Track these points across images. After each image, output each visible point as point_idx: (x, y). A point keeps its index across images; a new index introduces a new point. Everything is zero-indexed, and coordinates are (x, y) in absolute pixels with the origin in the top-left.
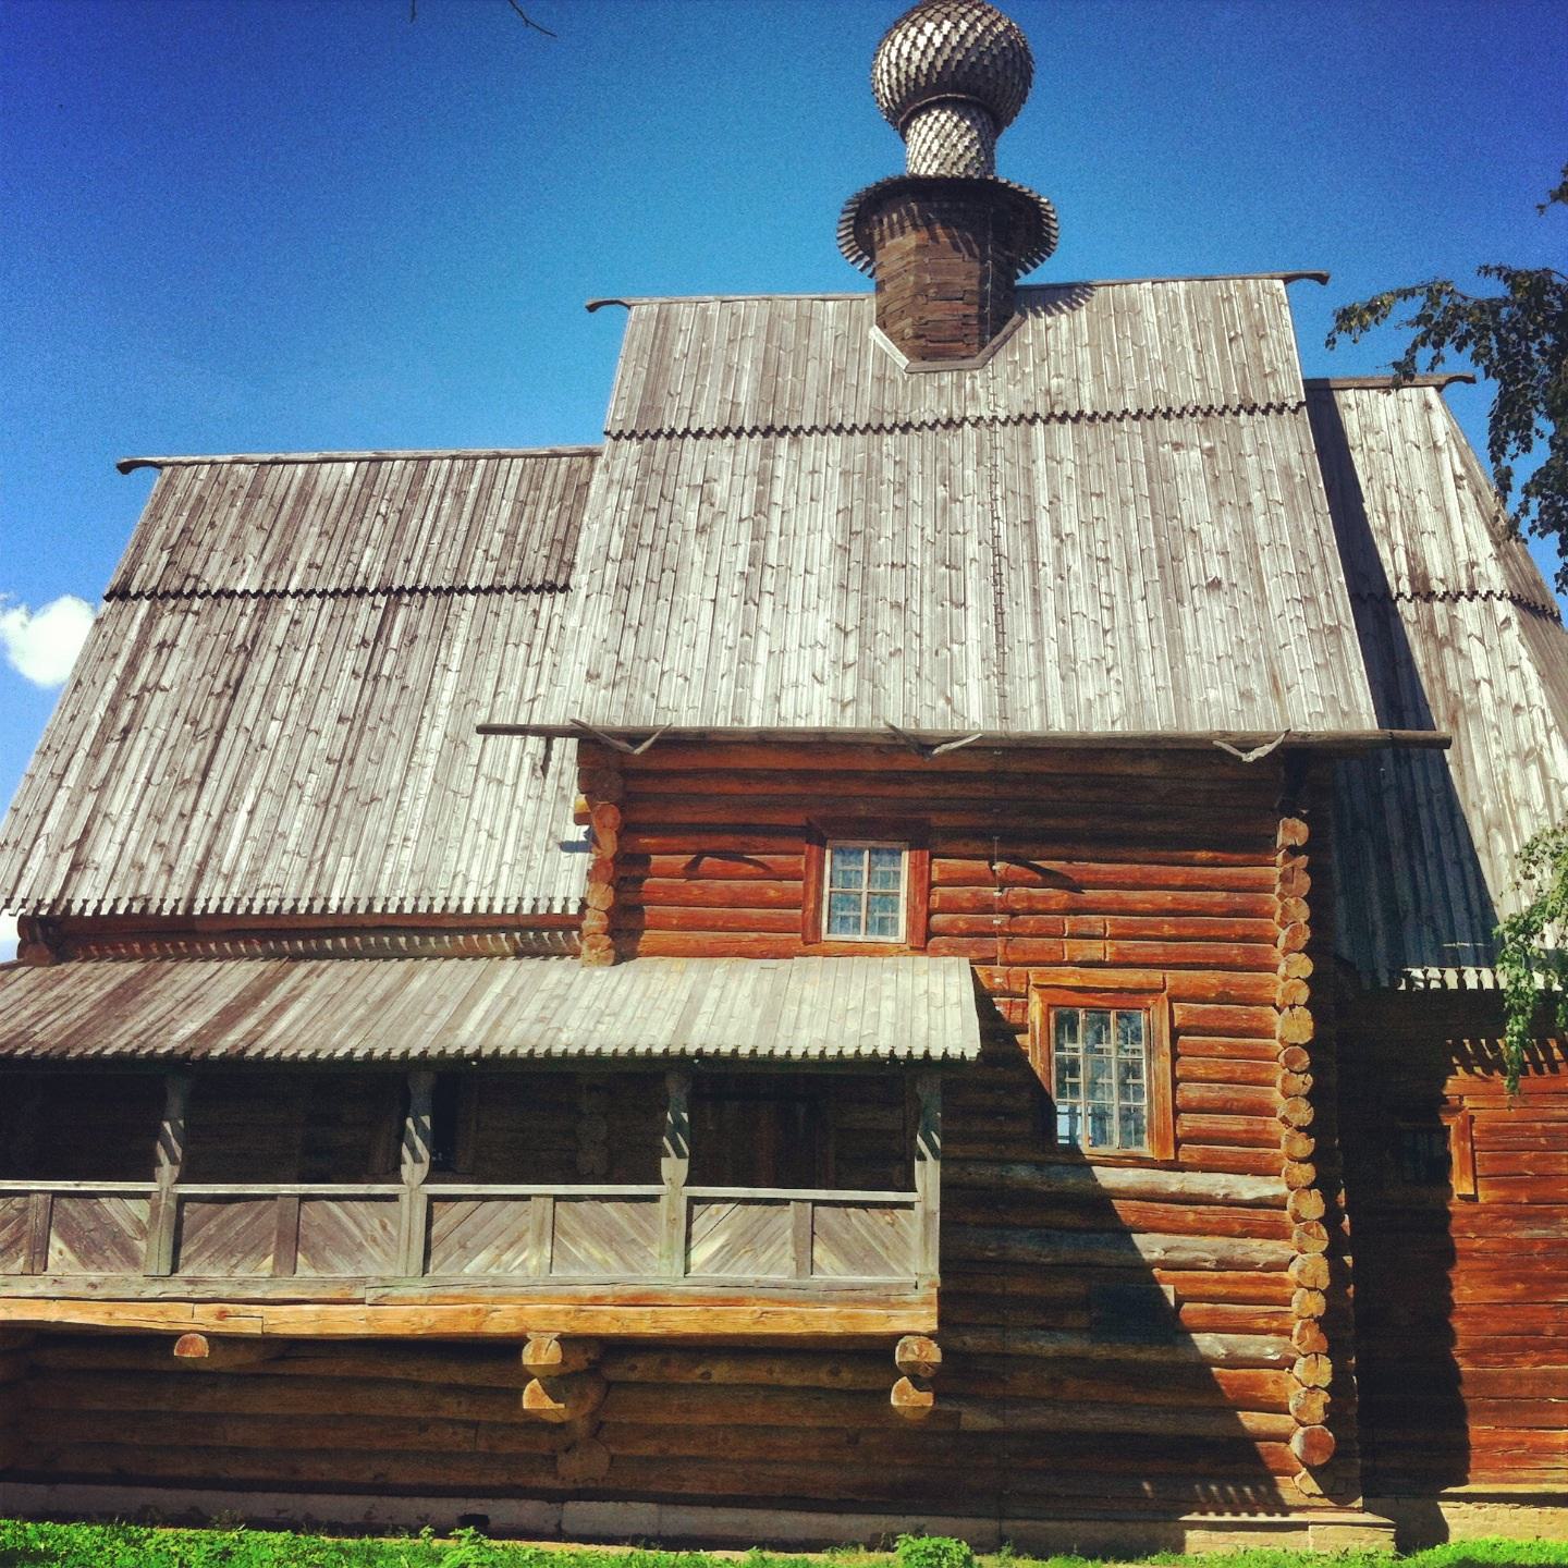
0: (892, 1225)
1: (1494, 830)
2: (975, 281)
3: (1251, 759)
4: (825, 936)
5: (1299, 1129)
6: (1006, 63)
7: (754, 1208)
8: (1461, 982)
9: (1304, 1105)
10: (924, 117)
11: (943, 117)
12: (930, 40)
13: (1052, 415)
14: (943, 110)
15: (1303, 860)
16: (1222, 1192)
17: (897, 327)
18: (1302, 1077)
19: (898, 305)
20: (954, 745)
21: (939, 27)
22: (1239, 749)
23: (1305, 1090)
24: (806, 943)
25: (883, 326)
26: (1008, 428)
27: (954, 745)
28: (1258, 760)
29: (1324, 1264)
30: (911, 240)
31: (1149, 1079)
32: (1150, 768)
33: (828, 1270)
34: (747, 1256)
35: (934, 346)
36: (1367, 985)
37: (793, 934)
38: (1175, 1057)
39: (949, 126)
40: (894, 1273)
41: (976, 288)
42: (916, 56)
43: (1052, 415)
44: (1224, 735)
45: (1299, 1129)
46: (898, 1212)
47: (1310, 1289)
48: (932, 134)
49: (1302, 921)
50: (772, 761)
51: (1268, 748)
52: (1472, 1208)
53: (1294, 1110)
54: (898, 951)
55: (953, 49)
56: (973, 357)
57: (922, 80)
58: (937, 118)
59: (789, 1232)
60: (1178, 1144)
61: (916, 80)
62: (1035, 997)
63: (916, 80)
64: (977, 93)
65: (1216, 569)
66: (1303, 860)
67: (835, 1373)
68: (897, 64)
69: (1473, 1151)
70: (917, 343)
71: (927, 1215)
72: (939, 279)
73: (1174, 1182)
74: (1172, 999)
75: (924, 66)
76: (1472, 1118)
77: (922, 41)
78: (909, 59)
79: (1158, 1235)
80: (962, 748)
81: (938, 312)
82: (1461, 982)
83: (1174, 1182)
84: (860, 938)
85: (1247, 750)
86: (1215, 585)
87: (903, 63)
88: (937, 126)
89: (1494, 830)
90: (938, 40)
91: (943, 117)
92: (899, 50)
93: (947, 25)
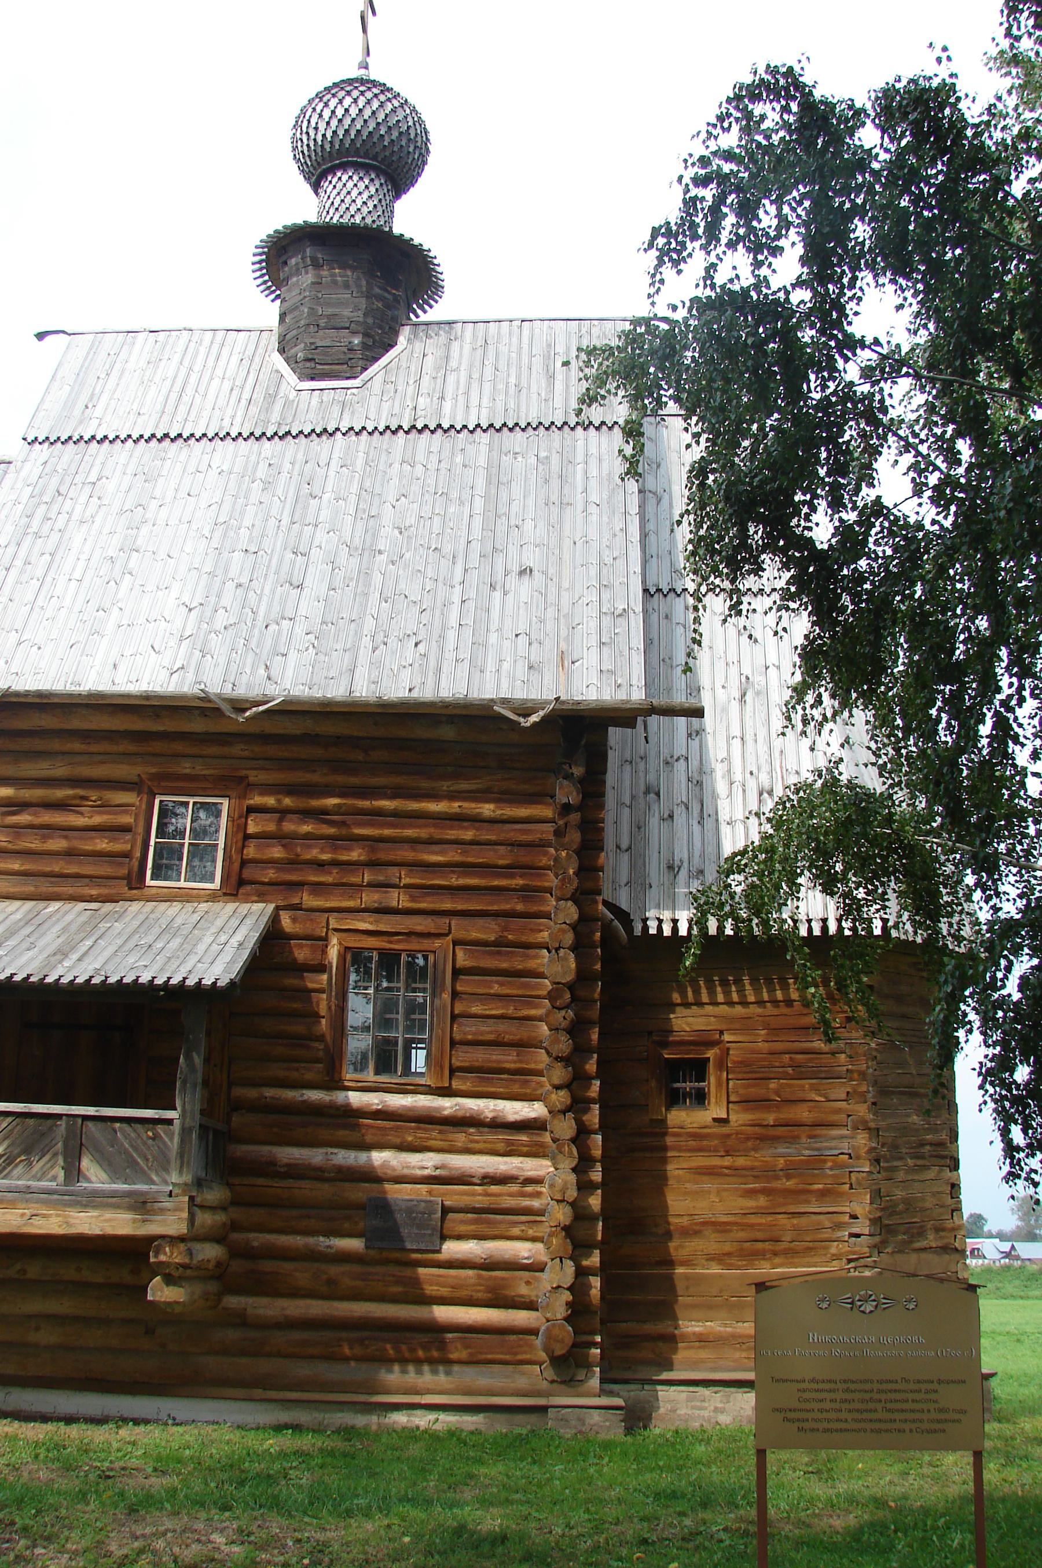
0: (153, 1139)
1: (765, 795)
2: (360, 313)
3: (528, 724)
4: (149, 882)
5: (557, 1059)
6: (401, 133)
7: (31, 1122)
8: (721, 928)
9: (563, 1037)
10: (339, 174)
11: (345, 178)
12: (333, 112)
13: (414, 427)
14: (367, 173)
15: (575, 817)
16: (490, 1115)
17: (293, 351)
18: (563, 1012)
19: (294, 333)
20: (261, 708)
21: (341, 102)
22: (519, 715)
23: (564, 1024)
24: (131, 888)
25: (282, 351)
26: (411, 436)
27: (261, 708)
28: (535, 724)
29: (572, 1178)
30: (308, 278)
31: (432, 1016)
32: (447, 733)
33: (94, 1179)
34: (21, 1166)
35: (316, 365)
36: (638, 930)
37: (121, 878)
38: (455, 995)
39: (350, 184)
40: (153, 1183)
41: (361, 319)
42: (322, 126)
43: (414, 427)
44: (505, 701)
45: (557, 1059)
46: (160, 1129)
47: (558, 1201)
48: (335, 192)
49: (571, 871)
50: (308, 726)
51: (541, 713)
52: (725, 1130)
53: (557, 1041)
54: (212, 897)
55: (340, 121)
56: (355, 378)
57: (327, 147)
58: (350, 177)
59: (60, 1145)
60: (452, 1071)
61: (322, 146)
62: (334, 941)
63: (322, 146)
64: (375, 158)
65: (531, 558)
66: (575, 817)
67: (79, 1270)
68: (307, 133)
69: (728, 1079)
70: (308, 364)
71: (185, 1131)
72: (330, 311)
73: (447, 1105)
74: (455, 943)
75: (329, 135)
76: (728, 1049)
77: (327, 114)
78: (316, 129)
79: (431, 1155)
80: (264, 712)
81: (324, 339)
82: (721, 928)
83: (447, 1105)
84: (182, 884)
85: (526, 715)
86: (525, 572)
87: (312, 133)
88: (340, 185)
89: (765, 795)
90: (340, 112)
91: (345, 178)
92: (309, 121)
93: (348, 101)
